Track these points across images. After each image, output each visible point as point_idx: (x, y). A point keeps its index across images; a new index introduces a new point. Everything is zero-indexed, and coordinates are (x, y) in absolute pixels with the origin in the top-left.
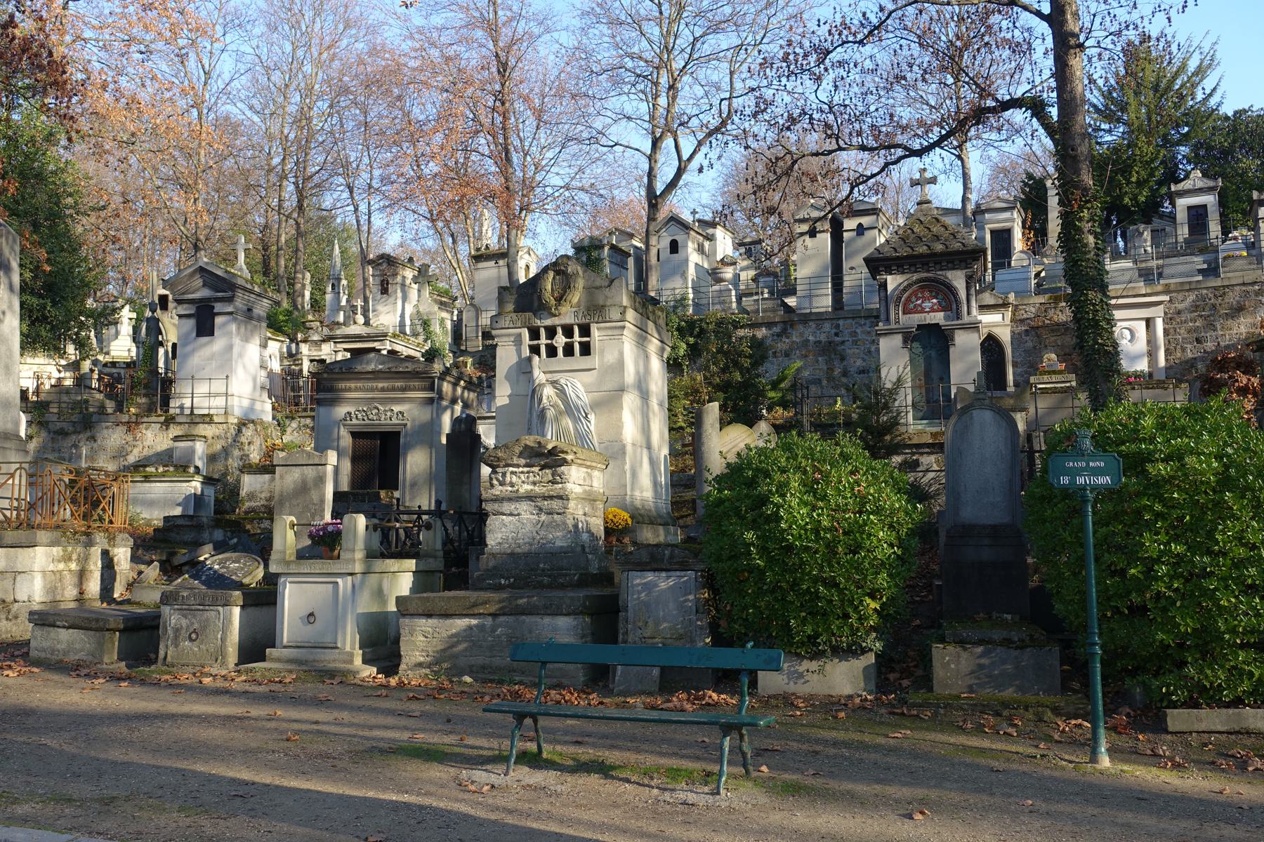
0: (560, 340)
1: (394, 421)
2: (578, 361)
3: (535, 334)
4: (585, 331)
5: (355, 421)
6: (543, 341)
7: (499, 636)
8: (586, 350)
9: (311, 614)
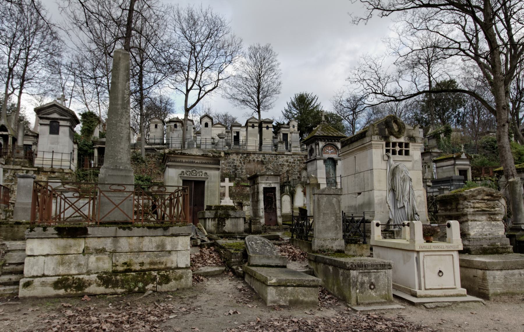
0: (398, 149)
1: (203, 176)
2: (403, 157)
3: (387, 145)
4: (407, 145)
5: (185, 175)
6: (391, 148)
8: (407, 153)
9: (440, 271)
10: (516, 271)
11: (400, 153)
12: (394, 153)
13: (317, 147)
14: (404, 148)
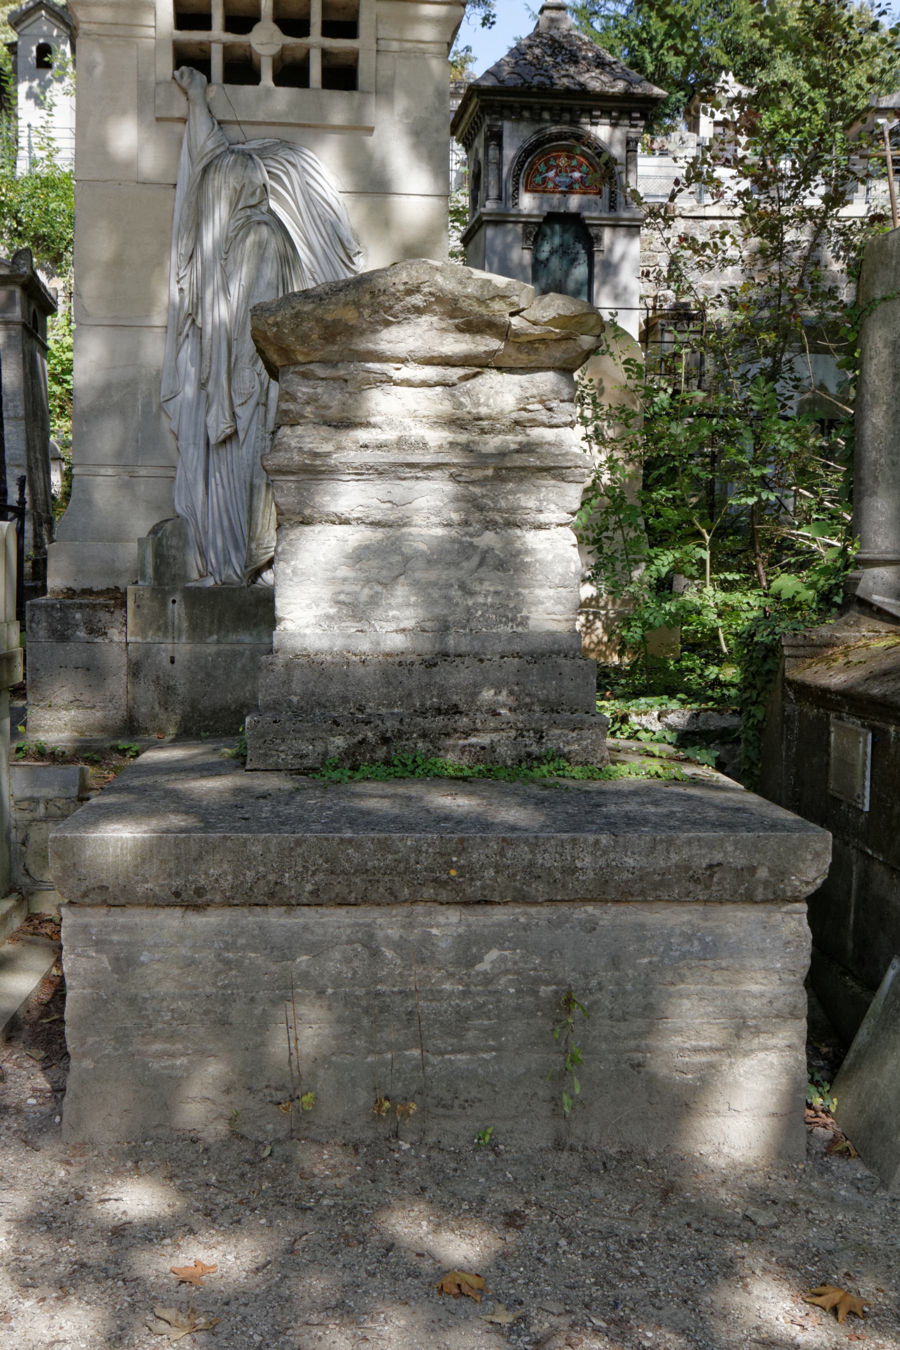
6: (217, 34)
7: (488, 979)
10: (336, 920)
11: (291, 73)
12: (242, 70)
13: (493, 152)
14: (316, 39)
